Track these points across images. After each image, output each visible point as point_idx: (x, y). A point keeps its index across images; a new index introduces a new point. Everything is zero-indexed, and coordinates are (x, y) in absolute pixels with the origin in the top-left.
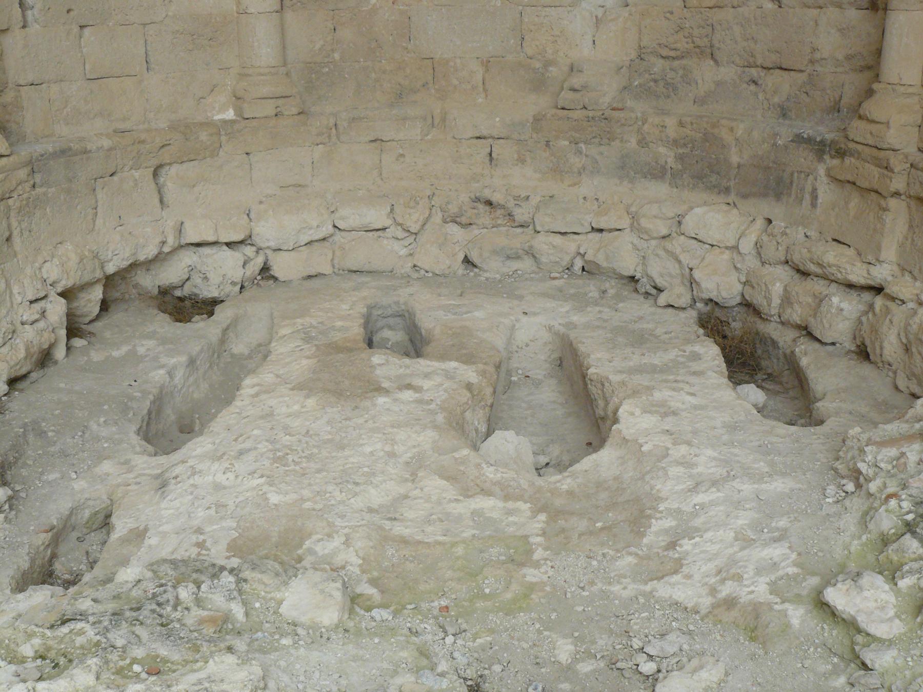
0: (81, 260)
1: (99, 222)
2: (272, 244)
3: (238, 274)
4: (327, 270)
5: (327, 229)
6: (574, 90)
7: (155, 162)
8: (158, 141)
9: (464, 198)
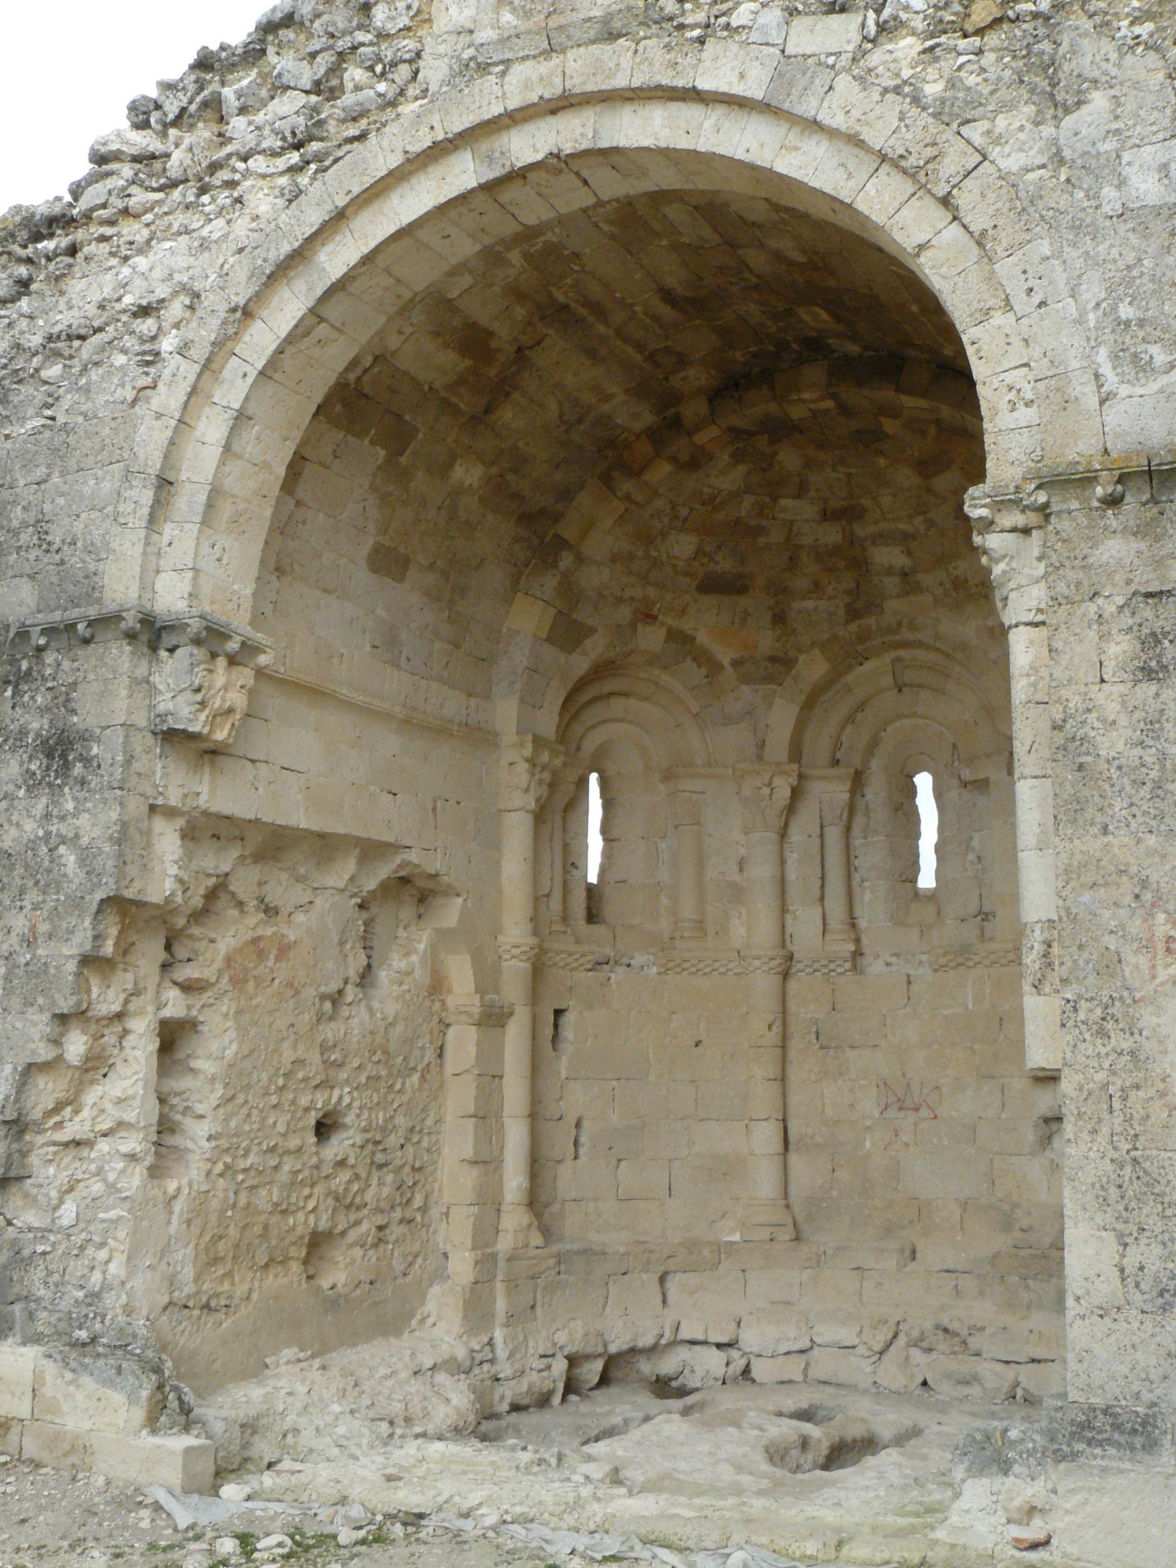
0: (586, 1334)
1: (608, 1309)
2: (755, 1350)
3: (720, 1371)
4: (799, 1377)
5: (805, 1343)
6: (1023, 1230)
7: (662, 1269)
8: (666, 1253)
9: (928, 1325)
